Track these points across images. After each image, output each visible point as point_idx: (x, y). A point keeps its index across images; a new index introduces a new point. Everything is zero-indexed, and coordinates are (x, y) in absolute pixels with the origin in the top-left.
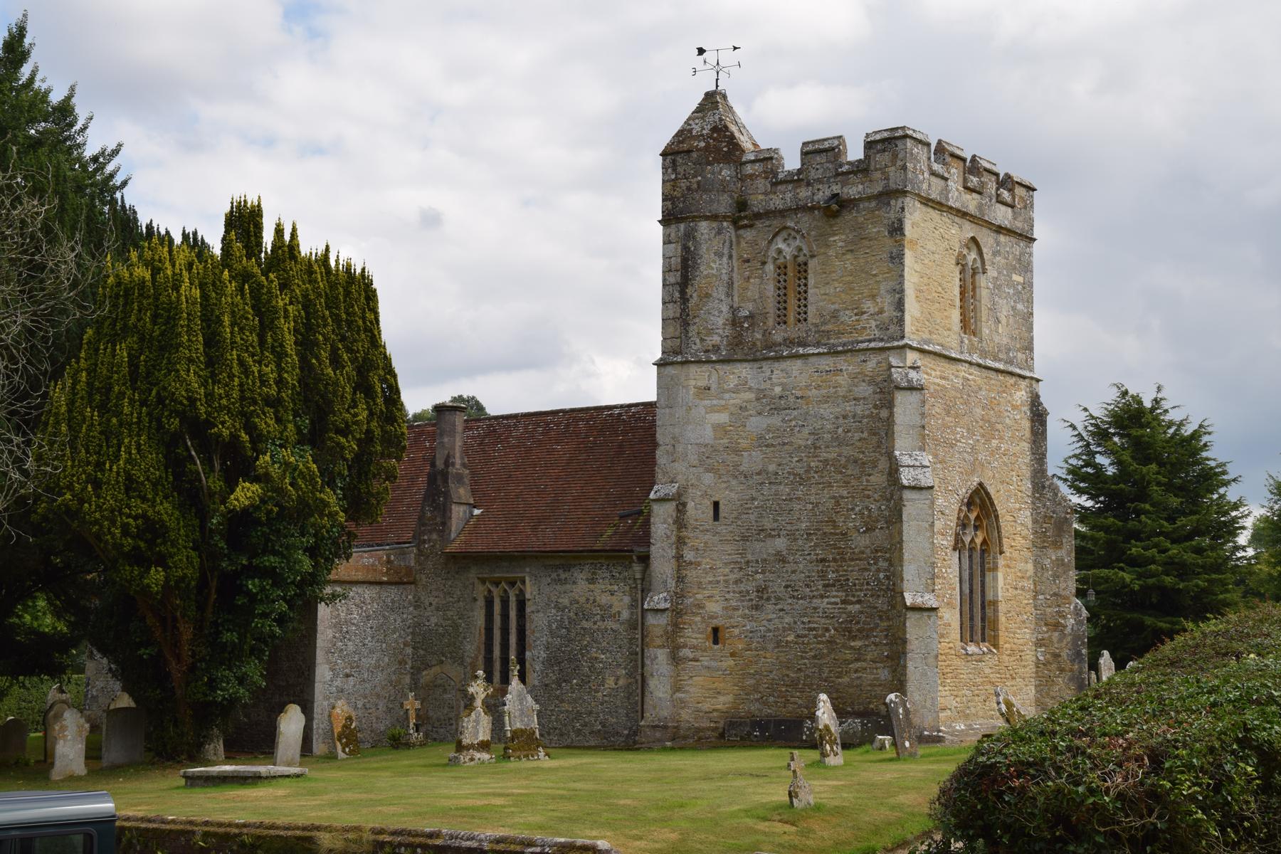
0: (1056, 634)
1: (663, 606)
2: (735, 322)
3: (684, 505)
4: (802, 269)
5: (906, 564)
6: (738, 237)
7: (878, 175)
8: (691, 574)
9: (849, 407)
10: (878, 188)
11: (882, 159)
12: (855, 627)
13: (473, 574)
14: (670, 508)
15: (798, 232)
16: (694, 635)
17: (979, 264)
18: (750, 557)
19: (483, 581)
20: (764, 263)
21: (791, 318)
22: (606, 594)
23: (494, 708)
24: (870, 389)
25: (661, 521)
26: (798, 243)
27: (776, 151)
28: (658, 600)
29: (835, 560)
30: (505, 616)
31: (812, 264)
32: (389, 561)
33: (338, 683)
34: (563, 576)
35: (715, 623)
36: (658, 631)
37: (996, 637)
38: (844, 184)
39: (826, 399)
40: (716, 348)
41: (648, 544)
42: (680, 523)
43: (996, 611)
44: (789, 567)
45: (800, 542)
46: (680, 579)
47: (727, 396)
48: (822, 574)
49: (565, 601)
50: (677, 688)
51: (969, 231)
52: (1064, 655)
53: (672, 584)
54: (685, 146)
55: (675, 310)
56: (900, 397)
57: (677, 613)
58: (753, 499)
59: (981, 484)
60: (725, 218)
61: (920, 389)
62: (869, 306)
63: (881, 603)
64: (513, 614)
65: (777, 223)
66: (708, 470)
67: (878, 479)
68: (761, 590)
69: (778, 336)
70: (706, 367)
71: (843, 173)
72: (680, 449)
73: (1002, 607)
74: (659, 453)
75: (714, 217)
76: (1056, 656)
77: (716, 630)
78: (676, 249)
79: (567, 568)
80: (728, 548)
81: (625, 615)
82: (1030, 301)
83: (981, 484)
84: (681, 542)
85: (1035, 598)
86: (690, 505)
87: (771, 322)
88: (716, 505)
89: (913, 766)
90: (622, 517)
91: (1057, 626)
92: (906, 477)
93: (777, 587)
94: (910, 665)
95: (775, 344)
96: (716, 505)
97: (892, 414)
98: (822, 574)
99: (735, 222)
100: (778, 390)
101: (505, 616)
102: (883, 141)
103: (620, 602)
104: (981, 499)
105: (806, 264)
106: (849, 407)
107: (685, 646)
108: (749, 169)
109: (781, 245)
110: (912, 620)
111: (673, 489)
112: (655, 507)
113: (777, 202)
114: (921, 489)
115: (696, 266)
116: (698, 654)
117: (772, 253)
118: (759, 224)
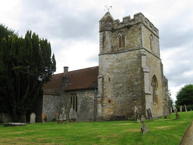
0: (166, 101)
1: (100, 96)
2: (112, 47)
3: (104, 79)
4: (124, 38)
5: (145, 86)
6: (112, 34)
7: (136, 21)
8: (105, 91)
9: (133, 60)
10: (136, 23)
11: (137, 18)
12: (135, 99)
13: (69, 93)
14: (101, 79)
15: (122, 32)
16: (106, 101)
17: (152, 39)
18: (115, 87)
19: (70, 94)
20: (117, 37)
21: (122, 46)
22: (90, 95)
23: (67, 113)
24: (137, 56)
25: (100, 81)
26: (123, 33)
27: (119, 19)
28: (99, 95)
29: (131, 87)
30: (74, 100)
31: (125, 37)
32: (56, 92)
33: (46, 111)
34: (83, 93)
35: (110, 99)
36: (99, 101)
37: (157, 101)
38: (131, 23)
39: (129, 59)
40: (109, 52)
41: (97, 86)
42: (103, 81)
43: (157, 97)
44: (123, 89)
45: (124, 84)
46: (103, 91)
47: (111, 60)
48: (129, 90)
49: (84, 97)
50: (103, 111)
51: (151, 33)
52: (167, 104)
53: (102, 92)
54: (103, 20)
55: (102, 46)
56: (142, 56)
57: (102, 97)
58: (116, 77)
59: (155, 75)
60: (110, 31)
61: (146, 55)
62: (136, 42)
63: (140, 94)
64: (75, 100)
65: (119, 31)
66: (108, 72)
67: (139, 72)
68: (117, 93)
69: (120, 49)
70: (108, 55)
71: (130, 21)
72: (103, 69)
73: (158, 96)
74: (99, 70)
75: (108, 30)
76: (166, 105)
77: (109, 100)
78: (102, 36)
79: (84, 92)
80: (112, 86)
81: (94, 99)
82: (159, 47)
83: (155, 75)
84: (103, 85)
85: (162, 95)
86: (105, 78)
87: (118, 47)
88: (109, 78)
89: (177, 122)
90: (93, 82)
91: (166, 100)
92: (144, 70)
93: (120, 92)
94: (146, 105)
95: (119, 51)
96: (109, 78)
97: (141, 60)
98: (129, 90)
99: (112, 31)
100: (120, 58)
101: (74, 100)
102: (137, 15)
103: (93, 97)
104: (155, 78)
105: (124, 37)
106: (133, 60)
107: (104, 103)
108: (114, 23)
109: (120, 34)
110: (146, 96)
111: (101, 76)
112: (99, 79)
113: (119, 27)
114: (147, 72)
115: (105, 38)
116: (106, 105)
117: (118, 36)
118: (116, 31)
